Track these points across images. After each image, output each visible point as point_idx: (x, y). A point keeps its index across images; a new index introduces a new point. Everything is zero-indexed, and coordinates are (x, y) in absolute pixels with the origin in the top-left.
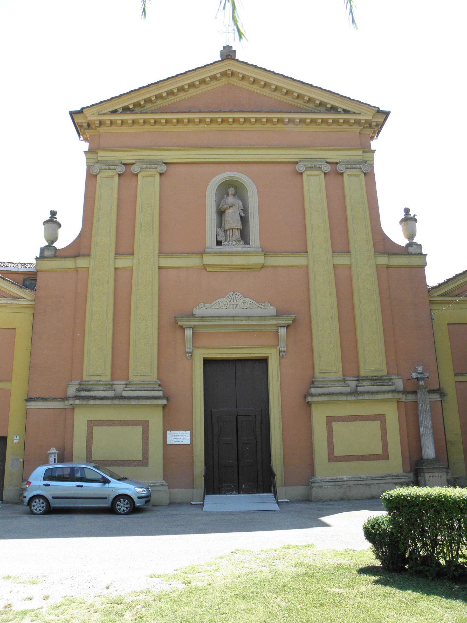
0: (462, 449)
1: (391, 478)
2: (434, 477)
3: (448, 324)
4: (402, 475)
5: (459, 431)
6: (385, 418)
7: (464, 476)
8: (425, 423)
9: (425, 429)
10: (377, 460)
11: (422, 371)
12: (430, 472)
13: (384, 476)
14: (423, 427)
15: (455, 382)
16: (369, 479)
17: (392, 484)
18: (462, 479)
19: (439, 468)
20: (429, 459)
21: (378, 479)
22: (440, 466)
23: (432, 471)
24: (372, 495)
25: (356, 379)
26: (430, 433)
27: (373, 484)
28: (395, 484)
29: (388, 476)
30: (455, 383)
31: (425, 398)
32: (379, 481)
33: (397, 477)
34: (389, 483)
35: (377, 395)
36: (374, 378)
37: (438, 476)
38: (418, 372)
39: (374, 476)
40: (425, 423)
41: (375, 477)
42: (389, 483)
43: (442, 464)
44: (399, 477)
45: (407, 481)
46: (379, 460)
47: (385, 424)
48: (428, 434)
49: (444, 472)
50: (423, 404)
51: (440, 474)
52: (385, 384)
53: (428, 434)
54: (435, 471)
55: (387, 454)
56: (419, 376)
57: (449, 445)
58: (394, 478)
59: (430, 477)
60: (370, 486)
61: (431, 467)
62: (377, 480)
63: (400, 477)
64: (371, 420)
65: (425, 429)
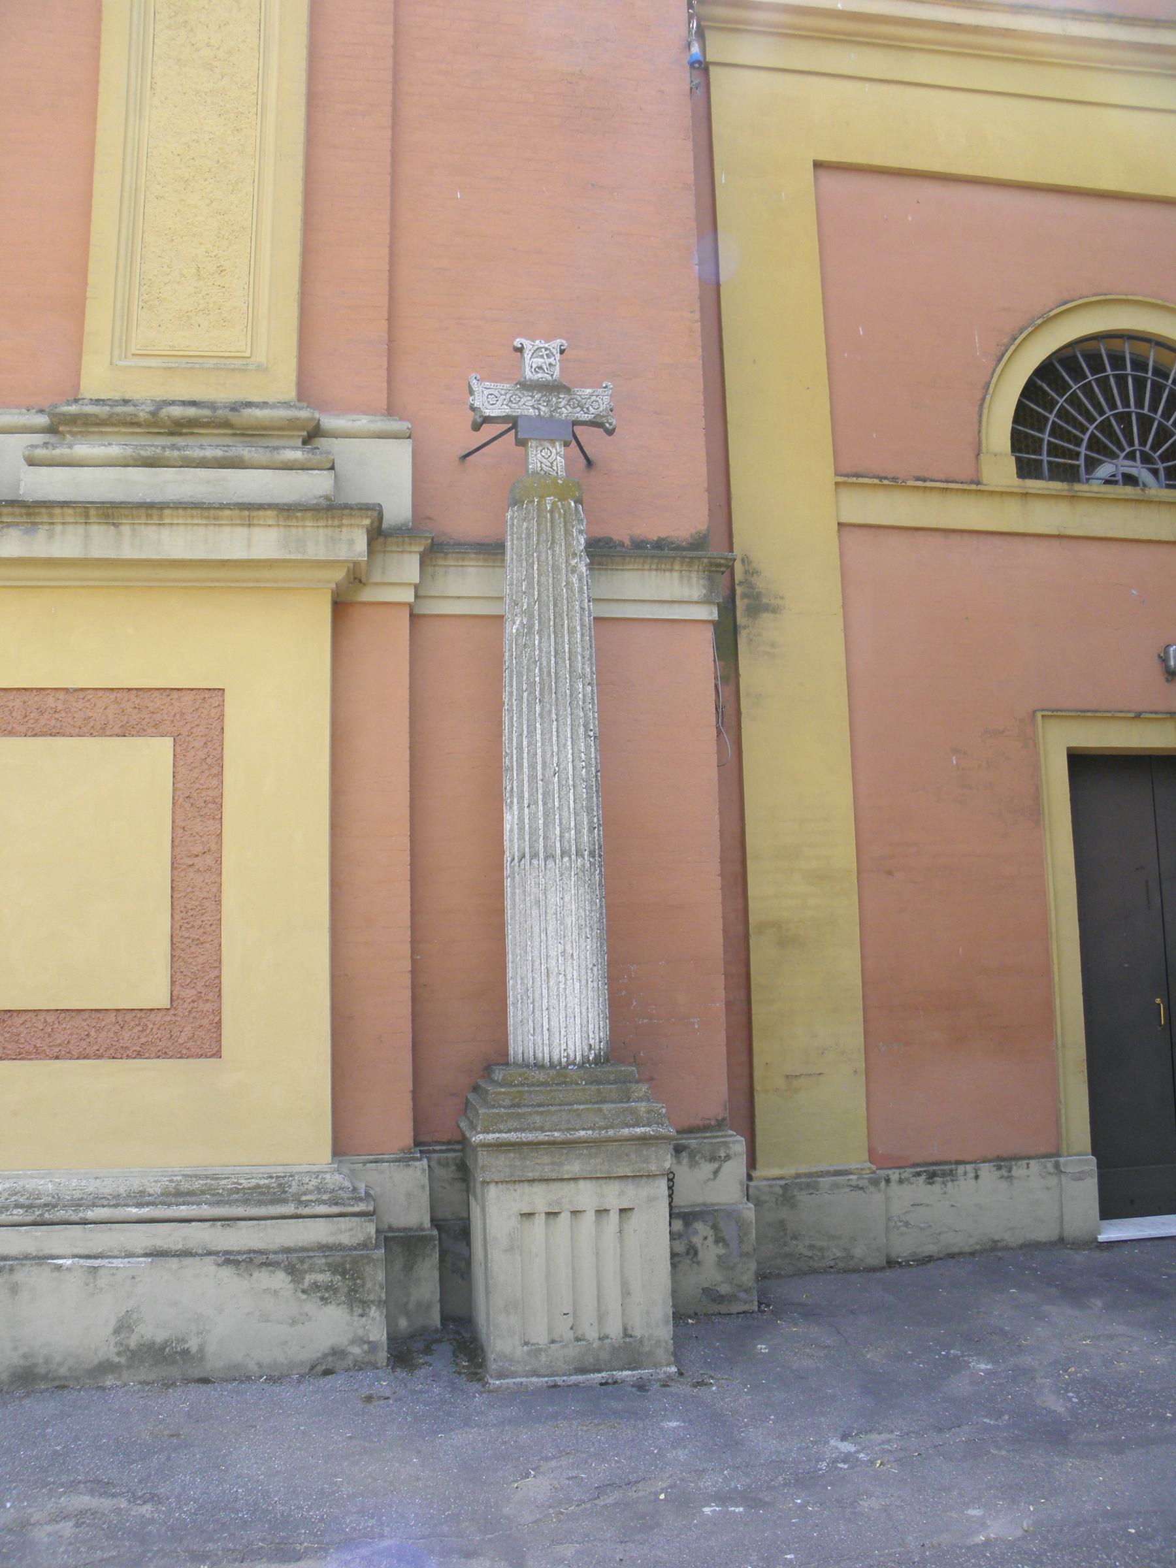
0: (855, 981)
1: (206, 1211)
2: (565, 1217)
3: (818, 165)
4: (318, 1189)
5: (844, 855)
6: (221, 717)
7: (853, 1166)
8: (533, 766)
9: (533, 818)
10: (116, 1053)
11: (557, 373)
12: (531, 1181)
13: (155, 1189)
14: (521, 798)
15: (839, 524)
16: (18, 1215)
17: (208, 1266)
18: (837, 1186)
19: (610, 1140)
20: (539, 1066)
21: (90, 1214)
22: (626, 1131)
23: (548, 1172)
24: (25, 1356)
25: (43, 420)
26: (564, 853)
27: (41, 1259)
28: (237, 1263)
29: (190, 1193)
30: (839, 531)
31: (556, 568)
32: (100, 1239)
33: (272, 1202)
34: (186, 1253)
35: (151, 533)
36: (177, 412)
37: (601, 1212)
38: (528, 374)
39: (72, 1185)
40: (533, 766)
41: (77, 1204)
42: (186, 1253)
43: (642, 1107)
44: (284, 1201)
45: (345, 1239)
46: (139, 1055)
47: (215, 765)
48: (549, 856)
49: (651, 1176)
50: (531, 617)
51: (613, 1196)
52: (246, 453)
53: (549, 856)
54: (574, 1167)
55: (208, 1007)
56: (527, 406)
57: (762, 954)
58: (239, 1211)
59: (530, 1215)
60: (20, 1276)
61: (541, 1137)
62: (84, 1222)
63: (290, 1209)
64: (102, 731)
65: (533, 818)
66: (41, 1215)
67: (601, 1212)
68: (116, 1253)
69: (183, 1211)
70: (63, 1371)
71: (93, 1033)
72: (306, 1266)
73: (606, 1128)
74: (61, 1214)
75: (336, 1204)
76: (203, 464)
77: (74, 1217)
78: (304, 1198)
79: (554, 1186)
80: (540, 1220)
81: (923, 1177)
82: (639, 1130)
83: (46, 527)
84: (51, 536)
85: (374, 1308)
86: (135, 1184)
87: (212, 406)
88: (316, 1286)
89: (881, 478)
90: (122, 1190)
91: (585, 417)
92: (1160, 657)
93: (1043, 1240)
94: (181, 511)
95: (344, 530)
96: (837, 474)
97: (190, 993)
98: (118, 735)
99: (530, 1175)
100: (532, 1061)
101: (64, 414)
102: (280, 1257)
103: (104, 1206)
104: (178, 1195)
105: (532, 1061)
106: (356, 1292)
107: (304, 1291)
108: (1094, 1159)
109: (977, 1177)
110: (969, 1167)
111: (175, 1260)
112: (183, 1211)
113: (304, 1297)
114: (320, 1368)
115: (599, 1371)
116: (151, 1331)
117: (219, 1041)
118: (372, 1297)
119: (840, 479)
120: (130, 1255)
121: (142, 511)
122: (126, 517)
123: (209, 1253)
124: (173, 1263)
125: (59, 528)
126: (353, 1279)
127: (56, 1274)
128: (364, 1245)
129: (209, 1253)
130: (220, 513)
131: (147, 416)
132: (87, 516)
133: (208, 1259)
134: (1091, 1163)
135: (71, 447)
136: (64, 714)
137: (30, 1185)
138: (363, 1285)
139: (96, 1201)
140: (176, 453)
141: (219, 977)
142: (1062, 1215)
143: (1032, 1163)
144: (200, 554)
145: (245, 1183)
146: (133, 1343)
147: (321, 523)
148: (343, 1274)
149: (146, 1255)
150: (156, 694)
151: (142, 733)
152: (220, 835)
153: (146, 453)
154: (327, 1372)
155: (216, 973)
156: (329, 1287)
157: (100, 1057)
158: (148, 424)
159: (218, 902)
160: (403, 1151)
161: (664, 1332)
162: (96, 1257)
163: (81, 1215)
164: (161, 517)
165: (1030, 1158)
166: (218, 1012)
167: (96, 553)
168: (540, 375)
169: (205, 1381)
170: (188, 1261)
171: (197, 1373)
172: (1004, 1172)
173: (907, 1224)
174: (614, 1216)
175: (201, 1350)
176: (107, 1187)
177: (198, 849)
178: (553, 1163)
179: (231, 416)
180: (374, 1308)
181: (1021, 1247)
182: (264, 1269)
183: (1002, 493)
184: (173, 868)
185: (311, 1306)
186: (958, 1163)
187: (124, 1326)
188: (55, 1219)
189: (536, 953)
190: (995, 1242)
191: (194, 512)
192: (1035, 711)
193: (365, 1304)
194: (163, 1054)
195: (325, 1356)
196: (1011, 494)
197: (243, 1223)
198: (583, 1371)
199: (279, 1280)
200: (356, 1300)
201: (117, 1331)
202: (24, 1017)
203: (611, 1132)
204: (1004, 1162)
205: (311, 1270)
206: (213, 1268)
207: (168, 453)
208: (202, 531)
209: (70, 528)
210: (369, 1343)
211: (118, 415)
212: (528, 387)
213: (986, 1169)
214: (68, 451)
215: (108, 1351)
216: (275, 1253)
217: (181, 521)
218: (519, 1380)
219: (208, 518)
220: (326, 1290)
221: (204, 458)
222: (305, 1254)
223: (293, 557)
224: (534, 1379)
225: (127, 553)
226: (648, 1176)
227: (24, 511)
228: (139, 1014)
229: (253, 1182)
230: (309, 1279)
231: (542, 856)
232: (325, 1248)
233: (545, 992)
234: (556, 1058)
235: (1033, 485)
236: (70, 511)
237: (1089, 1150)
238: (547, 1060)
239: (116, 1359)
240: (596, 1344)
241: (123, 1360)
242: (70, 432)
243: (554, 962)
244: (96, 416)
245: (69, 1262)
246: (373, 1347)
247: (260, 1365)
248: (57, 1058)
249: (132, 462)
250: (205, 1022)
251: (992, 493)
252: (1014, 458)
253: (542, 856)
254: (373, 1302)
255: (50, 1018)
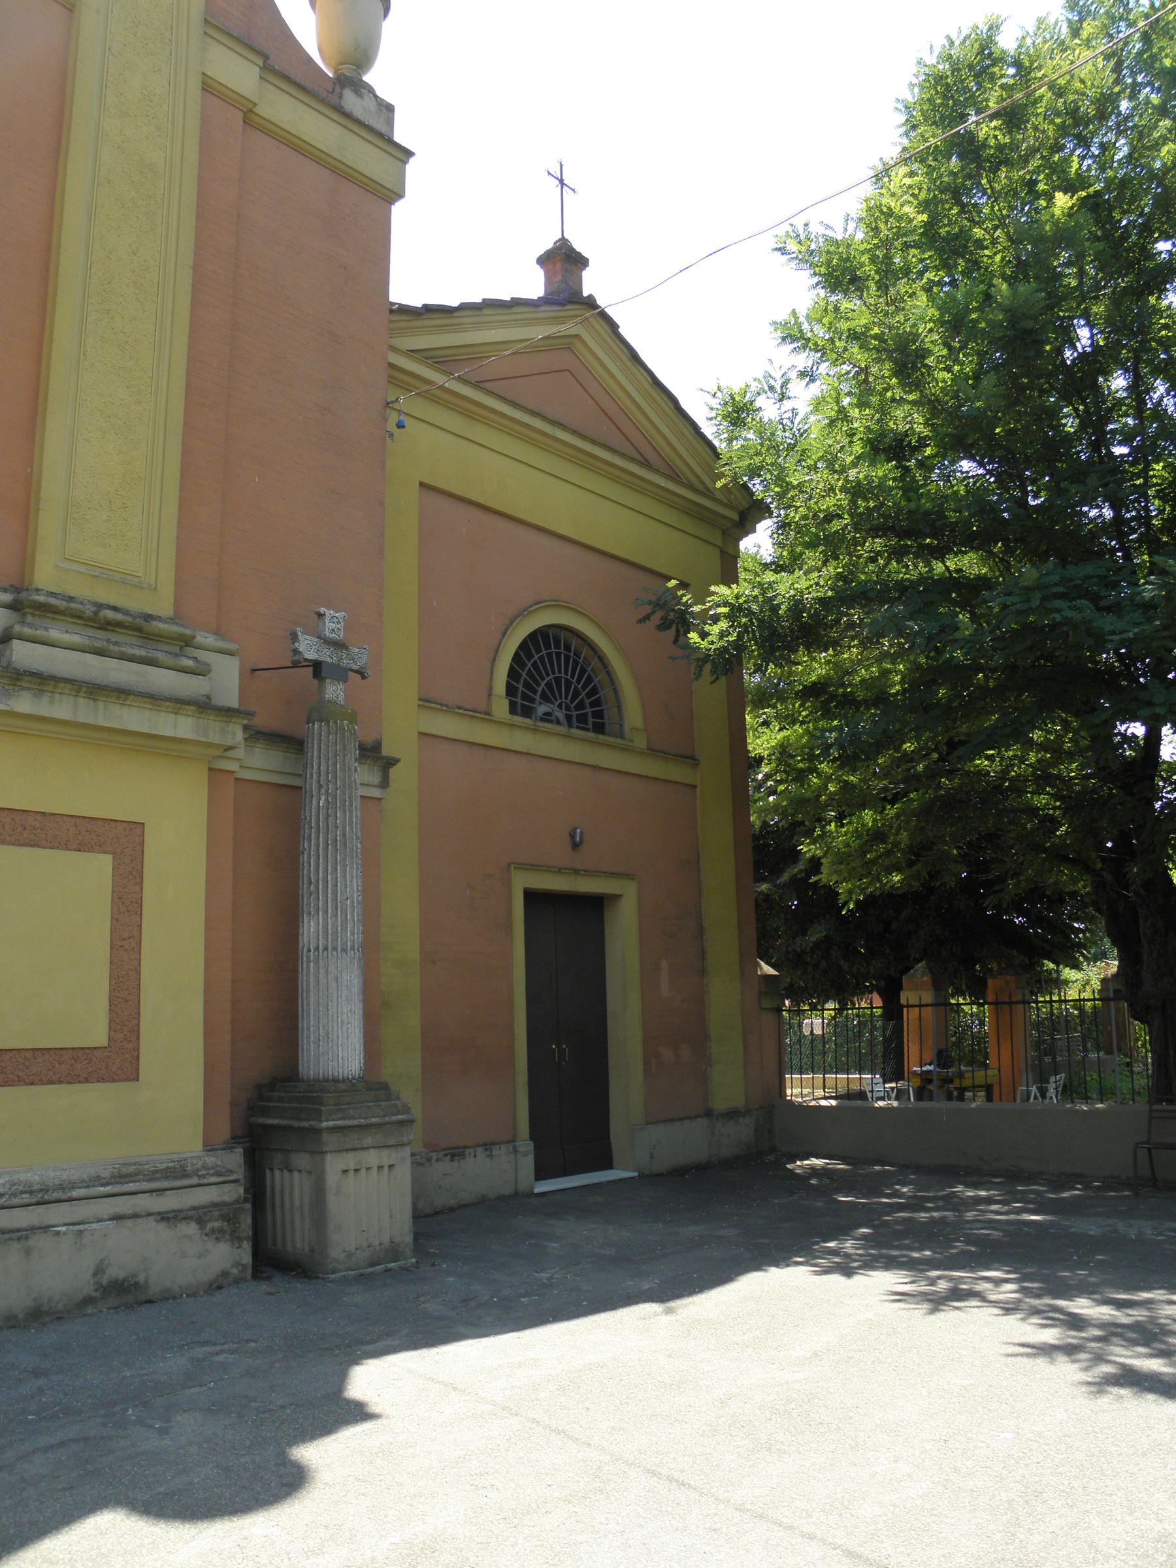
1: (146, 1186)
2: (363, 1171)
6: (142, 843)
9: (335, 926)
12: (347, 1150)
13: (106, 1174)
16: (26, 1198)
17: (151, 1223)
21: (75, 1193)
24: (35, 1299)
27: (46, 1228)
28: (167, 1219)
32: (81, 1211)
34: (135, 1216)
35: (116, 709)
36: (110, 614)
37: (380, 1168)
39: (54, 1176)
41: (61, 1187)
42: (135, 1216)
45: (227, 1198)
46: (87, 1081)
48: (344, 950)
51: (386, 1157)
53: (344, 950)
54: (368, 1141)
60: (31, 1242)
61: (356, 1122)
62: (71, 1200)
63: (195, 1181)
64: (65, 846)
65: (335, 926)
66: (43, 1197)
67: (380, 1168)
68: (91, 1220)
69: (132, 1187)
70: (60, 1307)
71: (57, 1065)
72: (208, 1218)
73: (384, 1116)
74: (55, 1195)
75: (221, 1175)
76: (132, 659)
77: (64, 1197)
78: (200, 1173)
79: (358, 1153)
80: (352, 1173)
81: (448, 1158)
82: (400, 1117)
83: (49, 694)
84: (52, 702)
85: (245, 1242)
86: (92, 1172)
87: (126, 612)
88: (213, 1231)
89: (441, 705)
90: (85, 1176)
91: (355, 667)
92: (570, 835)
93: (506, 1193)
94: (140, 698)
95: (230, 725)
96: (426, 702)
97: (120, 1036)
98: (75, 850)
99: (348, 1146)
100: (331, 1077)
101: (35, 602)
102: (193, 1213)
103: (80, 1188)
104: (120, 1178)
105: (331, 1077)
106: (235, 1231)
107: (206, 1235)
108: (532, 1143)
109: (475, 1156)
110: (471, 1150)
111: (132, 1220)
112: (132, 1187)
113: (206, 1238)
114: (215, 1285)
115: (380, 1264)
116: (116, 1272)
117: (138, 1069)
118: (244, 1235)
119: (421, 703)
120: (100, 1220)
121: (115, 694)
122: (104, 695)
123: (149, 1214)
124: (129, 1223)
125: (57, 696)
126: (234, 1224)
127: (56, 1238)
128: (237, 1201)
129: (149, 1214)
130: (163, 703)
131: (91, 614)
132: (78, 691)
133: (151, 1218)
134: (530, 1146)
135: (46, 629)
136: (39, 831)
137: (23, 1177)
138: (239, 1228)
139: (73, 1186)
140: (117, 648)
141: (138, 1025)
142: (516, 1179)
143: (503, 1146)
144: (145, 729)
145: (160, 1167)
146: (105, 1282)
147: (219, 719)
148: (228, 1221)
149: (110, 1219)
150: (101, 823)
151: (91, 849)
152: (140, 926)
153: (98, 644)
154: (220, 1287)
155: (135, 1022)
156: (221, 1231)
157: (60, 1082)
158: (89, 619)
159: (139, 973)
160: (224, 1142)
161: (409, 1239)
162: (79, 1224)
163: (69, 1195)
164: (125, 700)
165: (500, 1143)
166: (137, 1049)
167: (82, 719)
168: (333, 635)
169: (150, 1302)
170: (139, 1221)
171: (144, 1297)
172: (488, 1153)
173: (440, 1187)
174: (386, 1169)
175: (146, 1282)
176: (75, 1175)
177: (126, 935)
178: (359, 1139)
179: (144, 624)
180: (245, 1242)
181: (498, 1198)
182: (184, 1222)
183: (501, 723)
184: (111, 948)
185: (210, 1245)
186: (466, 1147)
187: (99, 1270)
188: (52, 1199)
189: (335, 1010)
190: (484, 1196)
191: (148, 700)
192: (509, 864)
193: (240, 1239)
194: (101, 1080)
195: (218, 1277)
196: (505, 724)
197: (168, 1192)
198: (372, 1265)
199: (192, 1228)
200: (235, 1238)
201: (95, 1274)
202: (9, 1054)
203: (387, 1119)
204: (488, 1146)
205: (210, 1220)
206: (154, 1224)
207: (111, 647)
208: (148, 713)
209: (64, 697)
210: (242, 1265)
211: (71, 609)
212: (329, 642)
213: (480, 1150)
214: (45, 633)
215: (89, 1289)
216: (188, 1210)
217: (137, 704)
218: (343, 1273)
219: (154, 705)
220: (219, 1232)
221: (134, 655)
222: (206, 1210)
223: (201, 739)
224: (350, 1272)
225: (101, 722)
226: (401, 1145)
227: (39, 681)
228: (88, 1052)
229: (165, 1165)
230: (210, 1225)
231: (339, 950)
232: (215, 1205)
233: (340, 1034)
234: (346, 1075)
235: (518, 719)
236: (69, 686)
237: (528, 1137)
238: (341, 1078)
239: (94, 1294)
240: (378, 1248)
241: (98, 1294)
242: (31, 614)
243: (345, 1016)
244: (57, 607)
245: (64, 1228)
246: (244, 1266)
247: (180, 1287)
248: (32, 1084)
249: (87, 650)
250: (128, 1056)
251: (496, 722)
252: (507, 701)
253: (339, 950)
254: (245, 1238)
255: (29, 1055)
